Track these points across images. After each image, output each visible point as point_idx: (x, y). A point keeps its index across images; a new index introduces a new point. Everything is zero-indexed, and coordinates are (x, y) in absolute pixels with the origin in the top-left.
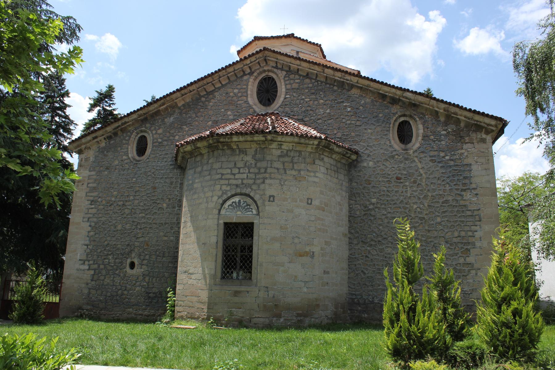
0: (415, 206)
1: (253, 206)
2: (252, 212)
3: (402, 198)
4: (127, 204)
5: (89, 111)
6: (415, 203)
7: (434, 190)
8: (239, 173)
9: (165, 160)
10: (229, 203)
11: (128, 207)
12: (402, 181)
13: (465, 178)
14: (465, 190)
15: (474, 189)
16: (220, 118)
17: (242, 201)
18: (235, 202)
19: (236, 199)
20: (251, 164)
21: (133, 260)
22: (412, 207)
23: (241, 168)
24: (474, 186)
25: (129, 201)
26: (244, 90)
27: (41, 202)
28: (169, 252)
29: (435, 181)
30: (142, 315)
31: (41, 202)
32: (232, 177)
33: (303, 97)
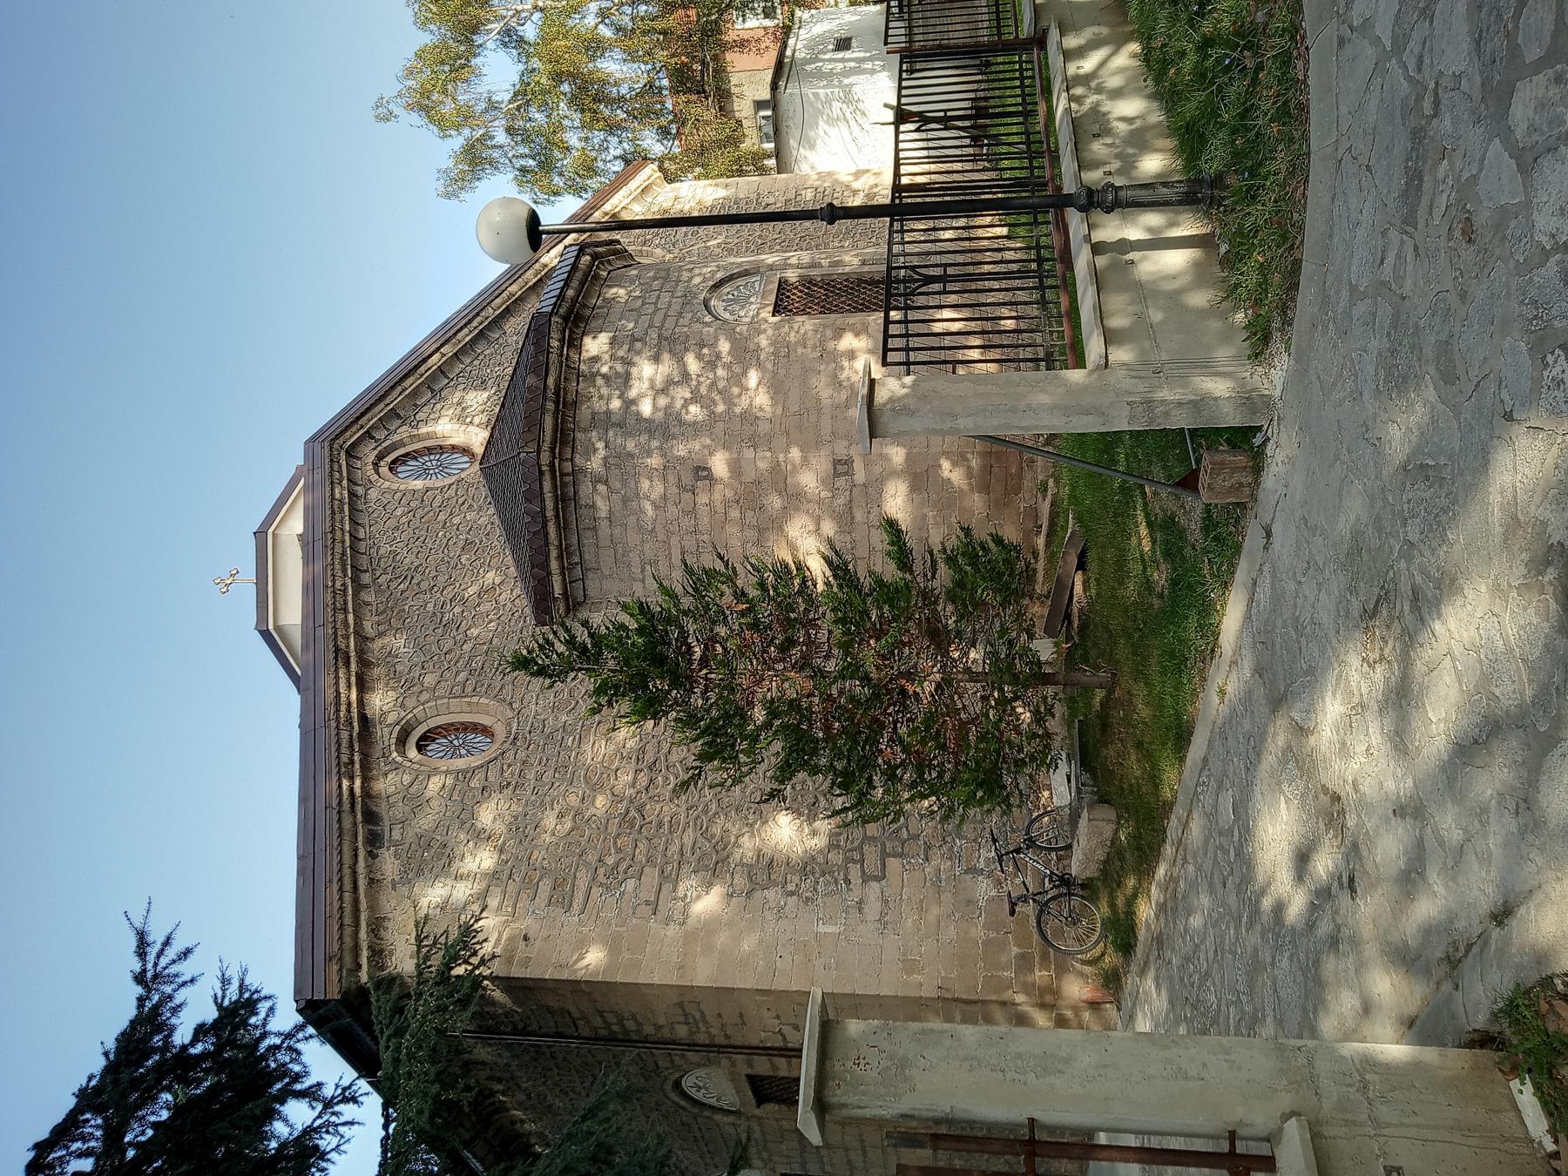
11: (665, 750)
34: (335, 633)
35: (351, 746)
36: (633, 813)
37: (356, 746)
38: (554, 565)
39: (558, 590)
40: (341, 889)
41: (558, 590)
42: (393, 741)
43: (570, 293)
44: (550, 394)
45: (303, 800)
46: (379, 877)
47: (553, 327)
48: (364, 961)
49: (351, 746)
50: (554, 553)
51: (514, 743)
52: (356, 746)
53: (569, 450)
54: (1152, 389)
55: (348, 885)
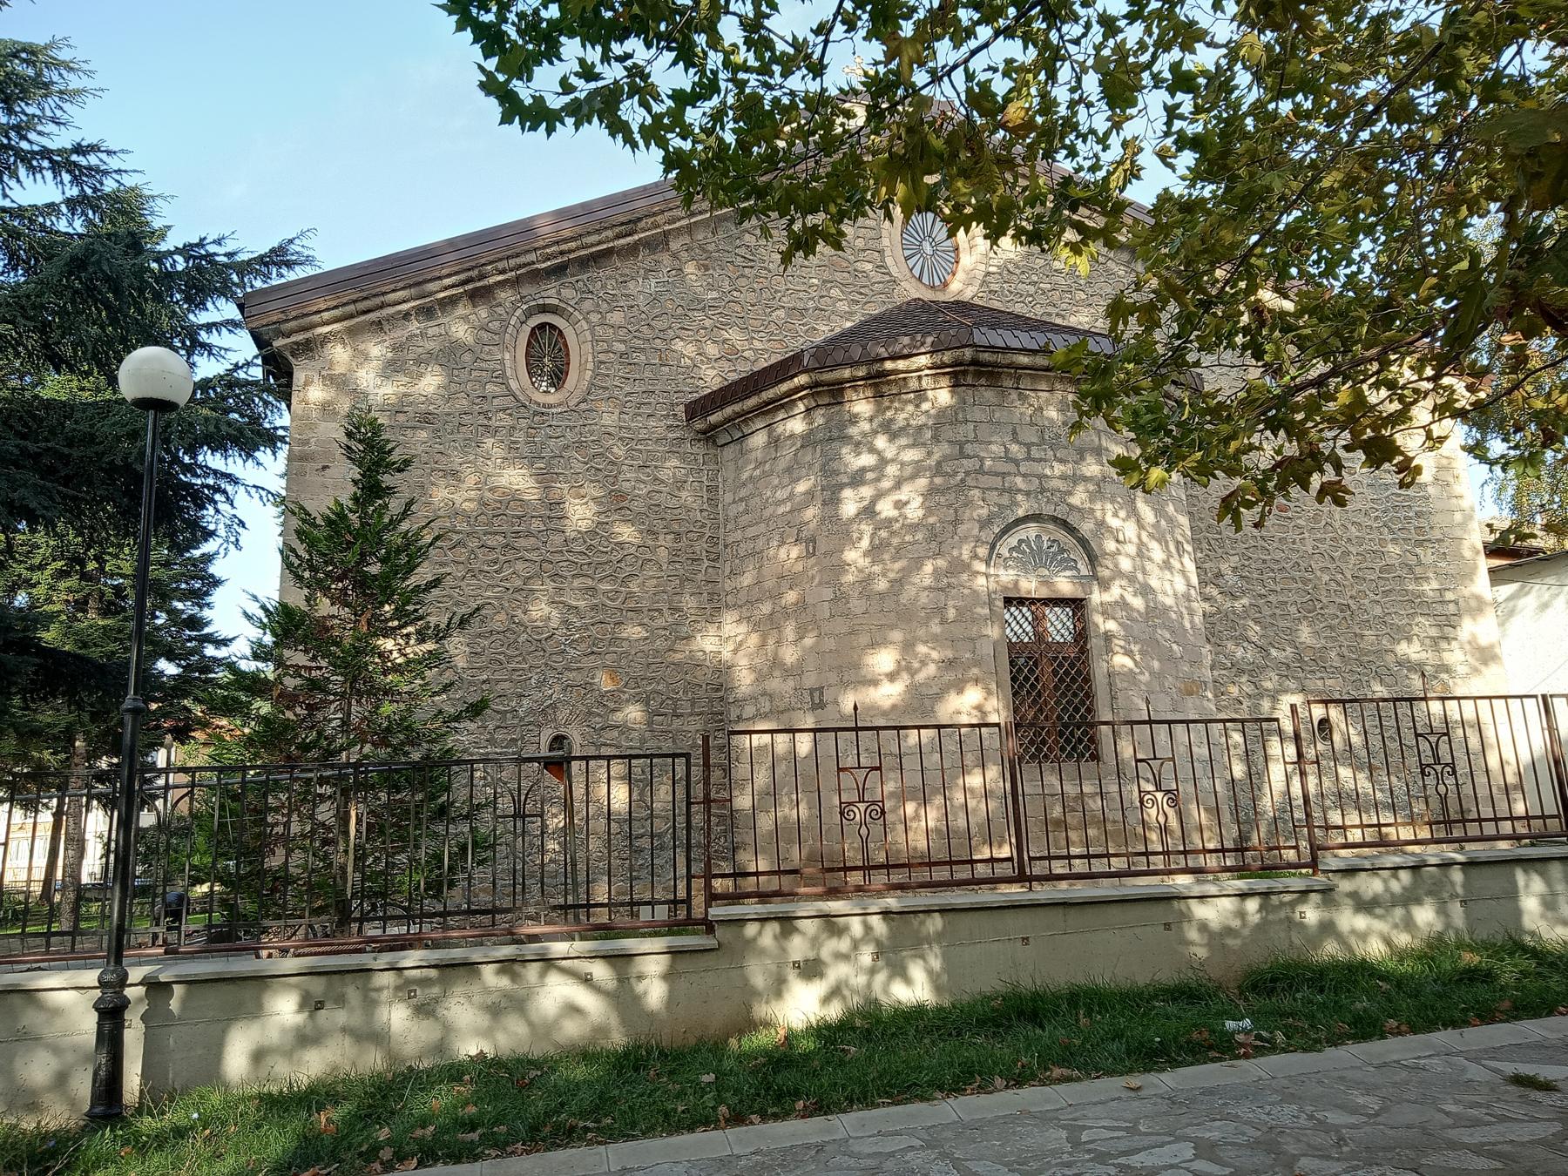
0: (1326, 578)
1: (1078, 554)
2: (1078, 570)
3: (1294, 557)
4: (522, 542)
5: (169, 227)
6: (1324, 569)
7: (1360, 541)
8: (1029, 458)
9: (645, 410)
10: (1013, 541)
11: (527, 555)
12: (1290, 514)
13: (1418, 515)
14: (1420, 543)
15: (1439, 541)
16: (811, 304)
17: (1045, 538)
18: (1027, 542)
19: (1031, 531)
20: (1058, 436)
21: (562, 731)
22: (1319, 579)
23: (1033, 444)
24: (1437, 534)
25: (529, 534)
26: (872, 234)
27: (1282, 433)
28: (693, 703)
29: (1361, 518)
30: (992, 860)
31: (1282, 433)
32: (1011, 468)
33: (1035, 278)
34: (655, 214)
35: (520, 267)
36: (456, 537)
37: (523, 271)
38: (729, 411)
39: (713, 419)
40: (354, 302)
41: (713, 419)
42: (541, 302)
43: (1024, 360)
44: (876, 367)
45: (625, 194)
46: (386, 328)
47: (958, 352)
48: (293, 339)
49: (520, 267)
50: (737, 408)
51: (536, 414)
52: (523, 271)
53: (827, 400)
54: (1454, 896)
55: (362, 306)
